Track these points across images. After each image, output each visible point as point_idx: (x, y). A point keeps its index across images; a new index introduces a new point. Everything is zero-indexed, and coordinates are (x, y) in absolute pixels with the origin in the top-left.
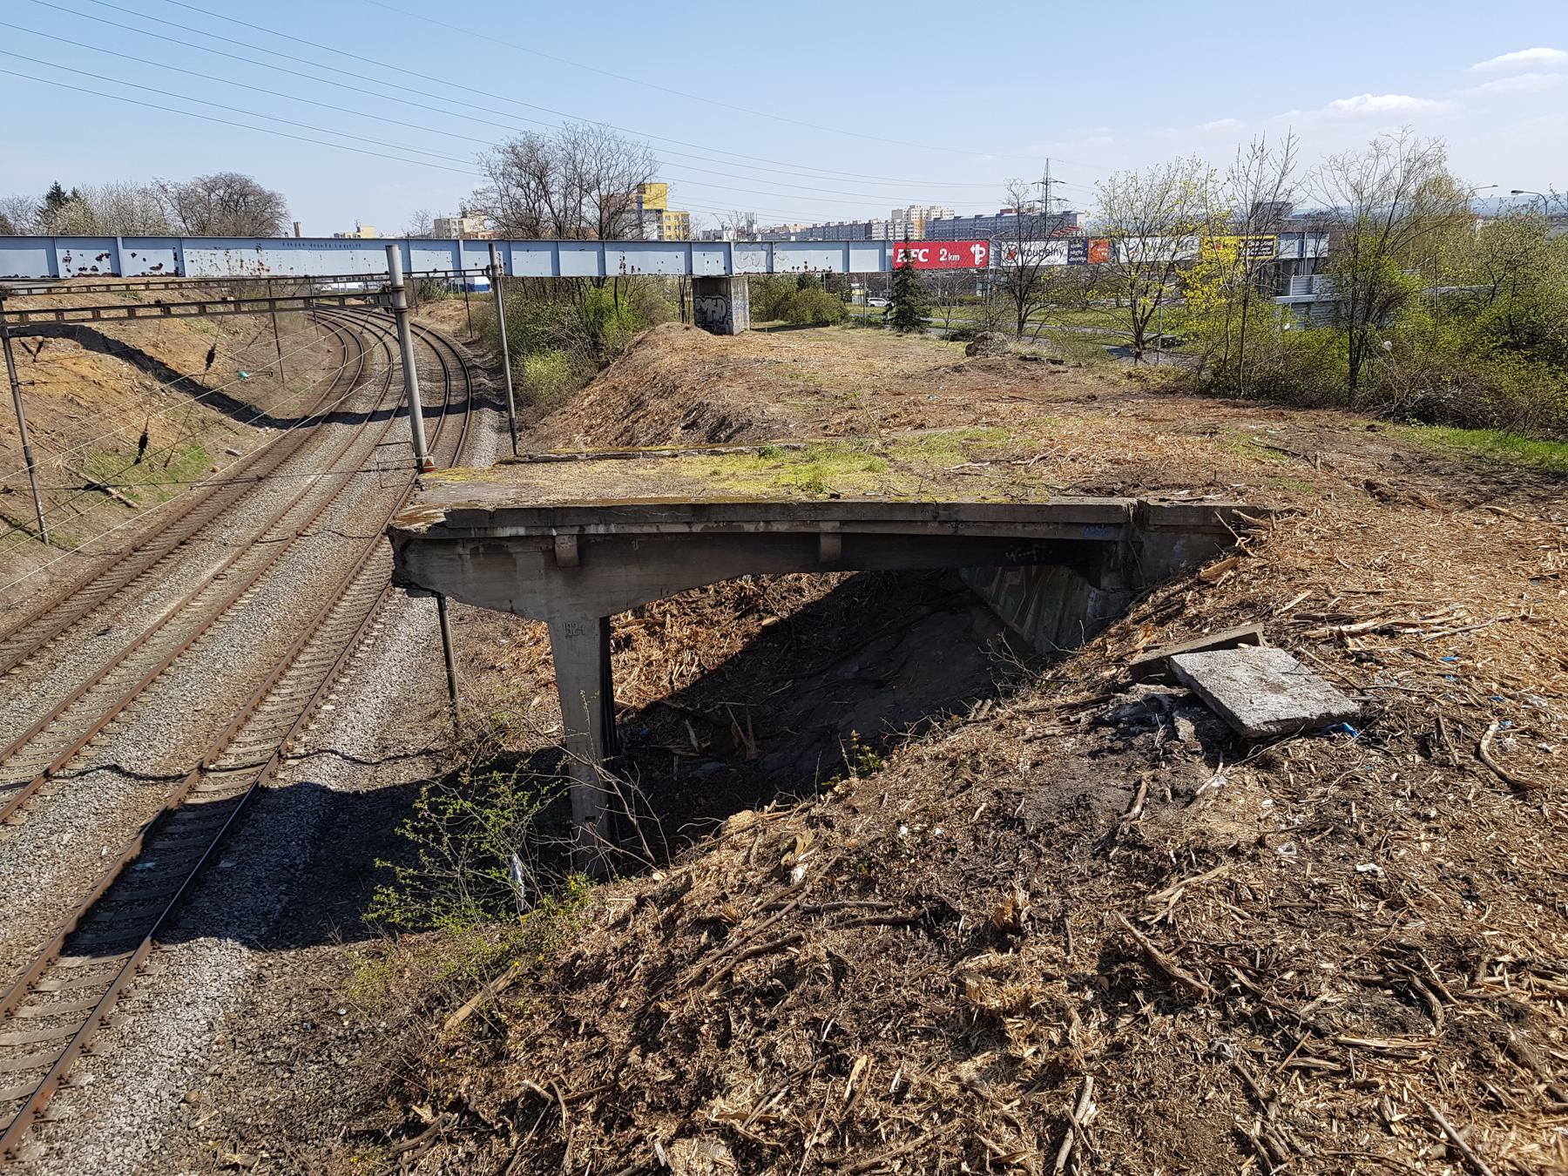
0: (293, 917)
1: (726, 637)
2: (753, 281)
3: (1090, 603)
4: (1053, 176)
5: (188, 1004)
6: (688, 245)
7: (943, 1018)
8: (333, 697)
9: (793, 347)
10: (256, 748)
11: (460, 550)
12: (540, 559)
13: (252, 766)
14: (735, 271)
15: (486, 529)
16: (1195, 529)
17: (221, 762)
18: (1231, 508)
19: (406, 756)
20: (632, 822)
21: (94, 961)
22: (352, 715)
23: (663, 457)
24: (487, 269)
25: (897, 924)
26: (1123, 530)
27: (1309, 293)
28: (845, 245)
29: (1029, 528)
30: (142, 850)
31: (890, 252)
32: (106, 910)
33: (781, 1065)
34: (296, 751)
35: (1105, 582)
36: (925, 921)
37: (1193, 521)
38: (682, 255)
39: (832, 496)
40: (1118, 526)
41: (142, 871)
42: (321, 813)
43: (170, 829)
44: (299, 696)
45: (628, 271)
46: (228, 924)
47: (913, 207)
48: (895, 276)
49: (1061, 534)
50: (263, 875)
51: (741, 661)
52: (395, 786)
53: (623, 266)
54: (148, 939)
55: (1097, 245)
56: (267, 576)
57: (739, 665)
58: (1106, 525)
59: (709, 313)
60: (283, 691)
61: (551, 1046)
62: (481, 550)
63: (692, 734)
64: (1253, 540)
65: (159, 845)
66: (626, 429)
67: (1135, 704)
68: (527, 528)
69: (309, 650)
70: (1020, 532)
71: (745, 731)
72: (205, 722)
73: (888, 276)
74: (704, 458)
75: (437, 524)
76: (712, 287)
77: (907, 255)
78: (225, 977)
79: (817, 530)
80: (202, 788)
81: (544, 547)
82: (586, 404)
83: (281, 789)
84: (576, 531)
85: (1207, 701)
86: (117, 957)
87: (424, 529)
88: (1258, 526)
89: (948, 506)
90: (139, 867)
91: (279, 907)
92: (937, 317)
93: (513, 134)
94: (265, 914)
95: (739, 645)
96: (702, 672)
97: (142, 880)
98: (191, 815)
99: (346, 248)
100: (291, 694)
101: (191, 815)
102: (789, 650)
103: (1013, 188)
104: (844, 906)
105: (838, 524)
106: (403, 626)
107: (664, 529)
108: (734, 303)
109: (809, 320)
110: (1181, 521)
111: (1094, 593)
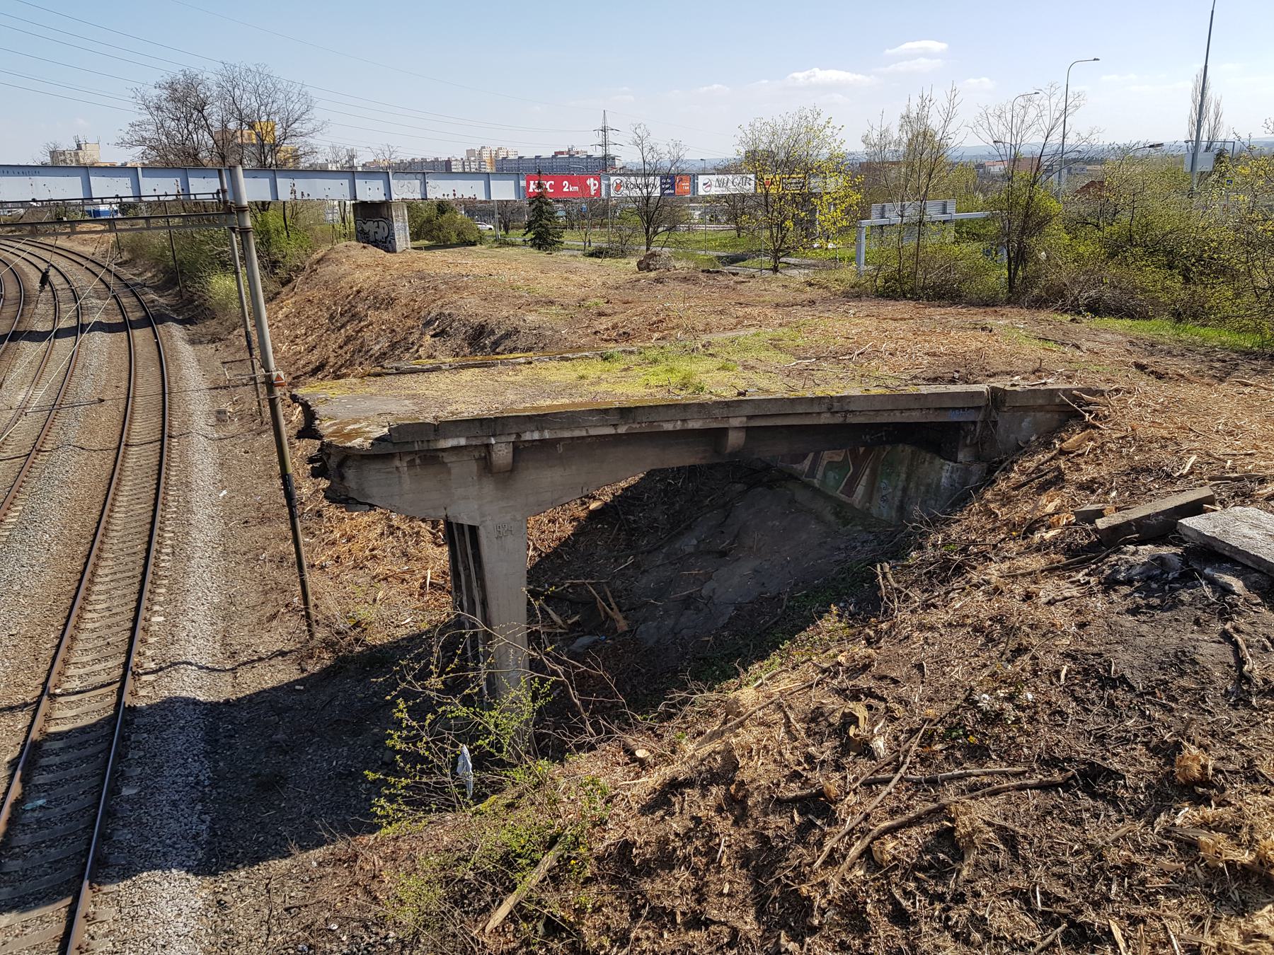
0: (223, 836)
1: (554, 522)
2: (410, 205)
3: (944, 474)
4: (610, 124)
5: (164, 946)
6: (350, 173)
7: (1178, 875)
8: (156, 608)
9: (440, 262)
10: (97, 667)
11: (397, 463)
12: (474, 467)
13: (103, 686)
14: (394, 197)
15: (428, 441)
16: (1041, 408)
17: (67, 686)
18: (1071, 390)
19: (260, 659)
20: (576, 704)
21: (25, 916)
22: (189, 625)
23: (519, 364)
24: (218, 193)
25: (1044, 787)
26: (983, 411)
27: (883, 217)
28: (515, 176)
29: (906, 414)
30: (23, 788)
31: (523, 183)
32: (11, 858)
33: (1004, 938)
34: (145, 666)
35: (961, 457)
36: (1076, 781)
37: (1040, 402)
38: (346, 182)
39: (740, 394)
40: (978, 408)
41: (33, 810)
42: (202, 725)
43: (44, 761)
44: (118, 610)
45: (299, 197)
46: (165, 854)
47: (484, 147)
48: (531, 204)
49: (932, 418)
50: (177, 797)
51: (575, 542)
52: (265, 691)
53: (293, 192)
54: (86, 883)
55: (681, 180)
56: (24, 494)
57: (573, 546)
58: (969, 408)
59: (372, 233)
60: (98, 607)
61: (648, 938)
62: (418, 461)
63: (550, 612)
64: (1097, 415)
65: (40, 779)
66: (349, 340)
67: (1144, 564)
68: (467, 438)
69: (104, 564)
70: (898, 418)
71: (609, 605)
72: (25, 646)
73: (526, 203)
74: (555, 363)
75: (377, 439)
76: (367, 211)
77: (539, 186)
78: (186, 910)
79: (726, 426)
80: (57, 714)
81: (477, 455)
82: (280, 316)
83: (150, 707)
84: (513, 438)
85: (1238, 558)
86: (51, 907)
87: (367, 445)
88: (1096, 404)
89: (841, 399)
90: (29, 806)
91: (204, 827)
92: (569, 238)
93: (173, 68)
94: (194, 837)
95: (569, 529)
96: (540, 555)
97: (38, 821)
98: (58, 745)
99: (24, 174)
100: (109, 609)
101: (58, 745)
102: (619, 529)
103: (638, 131)
104: (970, 775)
105: (745, 419)
106: (195, 533)
107: (593, 432)
108: (395, 225)
109: (454, 239)
110: (1031, 403)
111: (949, 466)
